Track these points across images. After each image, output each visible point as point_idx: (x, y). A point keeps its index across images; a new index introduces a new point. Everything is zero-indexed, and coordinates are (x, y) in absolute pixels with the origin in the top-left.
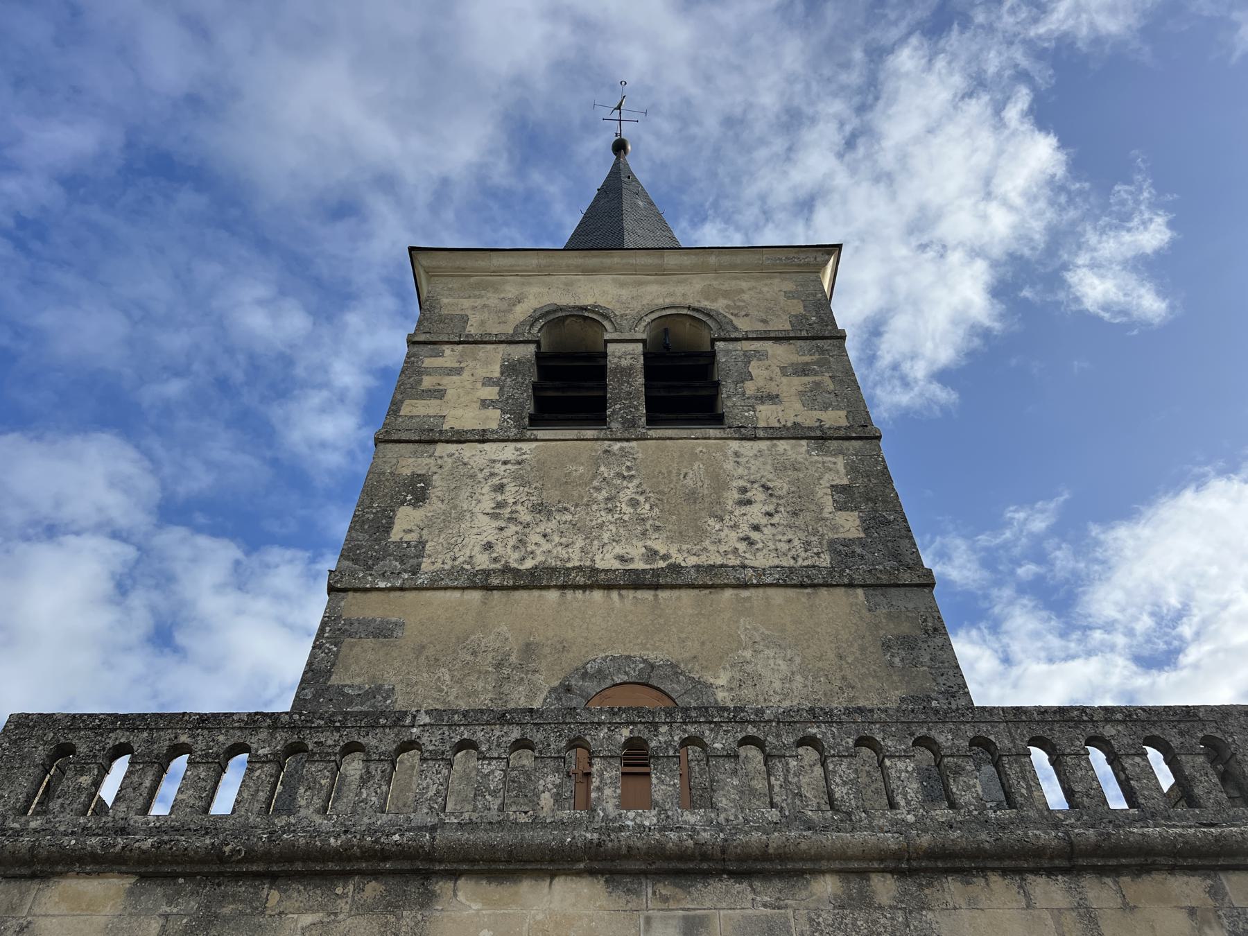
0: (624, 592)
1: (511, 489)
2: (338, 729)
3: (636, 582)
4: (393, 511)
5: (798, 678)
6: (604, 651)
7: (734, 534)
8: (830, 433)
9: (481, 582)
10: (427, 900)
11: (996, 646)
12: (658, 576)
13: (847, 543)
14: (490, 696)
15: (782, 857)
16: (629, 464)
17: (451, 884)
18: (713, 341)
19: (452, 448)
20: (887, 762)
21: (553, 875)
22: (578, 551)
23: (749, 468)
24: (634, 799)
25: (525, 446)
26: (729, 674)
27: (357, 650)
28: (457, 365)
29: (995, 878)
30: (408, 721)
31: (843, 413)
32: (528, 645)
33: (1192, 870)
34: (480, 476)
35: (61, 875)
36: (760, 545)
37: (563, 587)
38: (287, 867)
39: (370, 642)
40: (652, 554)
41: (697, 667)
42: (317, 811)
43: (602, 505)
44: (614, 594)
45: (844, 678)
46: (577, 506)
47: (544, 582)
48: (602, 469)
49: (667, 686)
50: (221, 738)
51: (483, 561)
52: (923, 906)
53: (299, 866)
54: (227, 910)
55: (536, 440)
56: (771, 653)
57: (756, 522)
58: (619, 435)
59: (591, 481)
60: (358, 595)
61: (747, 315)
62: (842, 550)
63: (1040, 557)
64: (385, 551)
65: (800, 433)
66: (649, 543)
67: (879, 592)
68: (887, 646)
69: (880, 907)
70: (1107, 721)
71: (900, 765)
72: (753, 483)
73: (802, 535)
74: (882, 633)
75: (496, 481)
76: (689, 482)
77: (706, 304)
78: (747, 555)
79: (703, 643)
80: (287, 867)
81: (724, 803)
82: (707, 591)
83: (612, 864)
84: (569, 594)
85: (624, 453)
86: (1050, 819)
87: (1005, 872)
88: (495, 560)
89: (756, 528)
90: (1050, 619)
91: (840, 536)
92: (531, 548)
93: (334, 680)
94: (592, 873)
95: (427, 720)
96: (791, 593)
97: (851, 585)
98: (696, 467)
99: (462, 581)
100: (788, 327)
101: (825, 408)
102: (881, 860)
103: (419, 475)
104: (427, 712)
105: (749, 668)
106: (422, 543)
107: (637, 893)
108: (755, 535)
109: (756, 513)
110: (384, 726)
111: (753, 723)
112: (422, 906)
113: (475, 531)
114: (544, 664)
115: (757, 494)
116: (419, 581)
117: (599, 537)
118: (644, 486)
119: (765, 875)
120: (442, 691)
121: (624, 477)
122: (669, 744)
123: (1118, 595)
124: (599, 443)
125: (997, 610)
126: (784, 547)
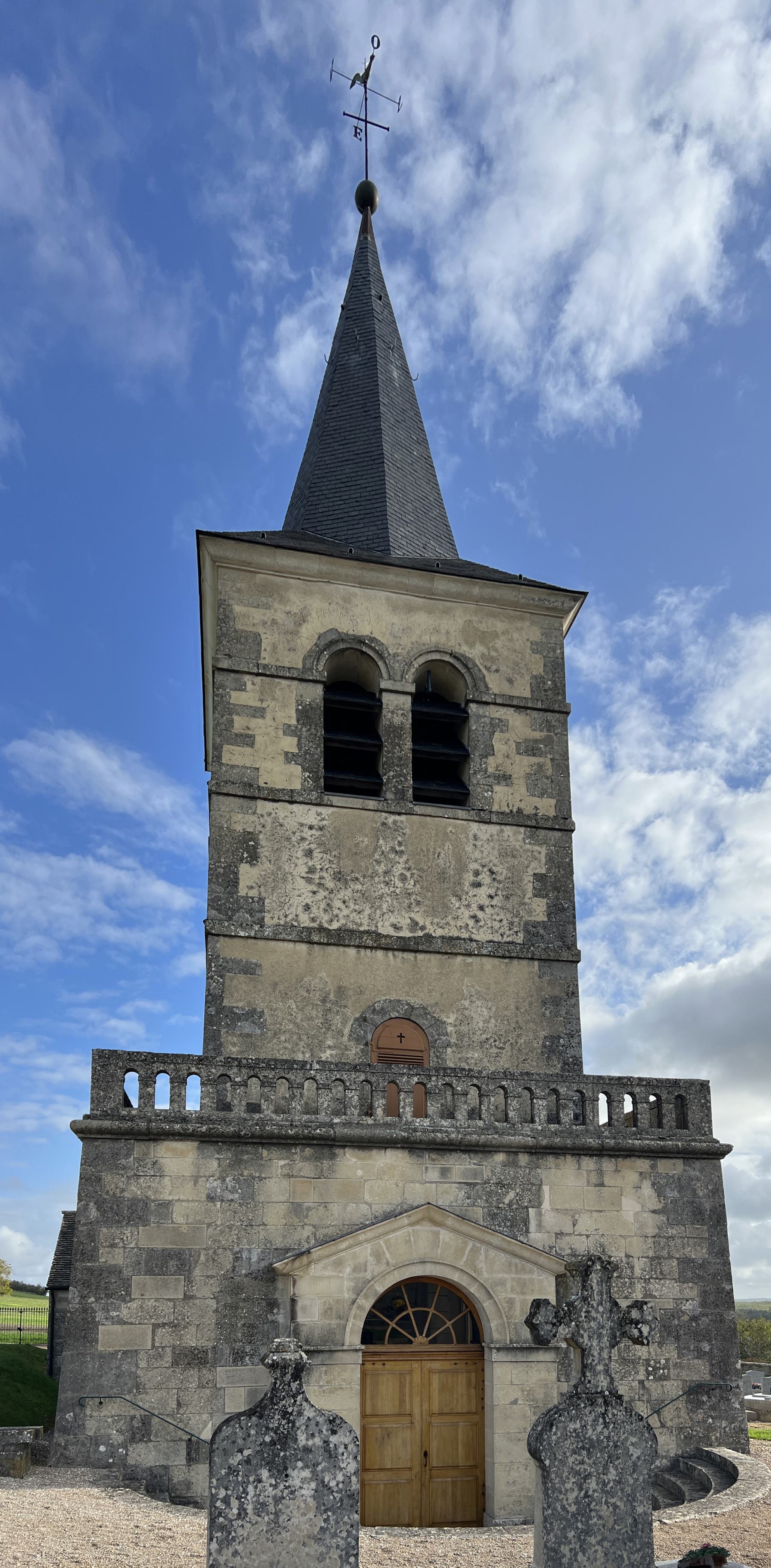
0: (396, 953)
1: (317, 854)
2: (273, 1069)
3: (405, 946)
4: (236, 867)
5: (493, 1021)
6: (384, 995)
7: (467, 912)
8: (542, 823)
9: (306, 936)
10: (333, 1156)
11: (603, 748)
12: (418, 943)
13: (535, 925)
14: (321, 1021)
15: (484, 1146)
16: (400, 839)
17: (342, 1150)
18: (468, 702)
19: (269, 806)
20: (535, 1101)
21: (386, 1148)
22: (367, 917)
23: (482, 852)
24: (420, 1112)
25: (326, 811)
26: (455, 1016)
27: (235, 982)
28: (258, 704)
29: (569, 1158)
30: (308, 1067)
31: (553, 802)
32: (340, 988)
33: (648, 1157)
34: (294, 839)
35: (164, 1140)
36: (482, 923)
37: (358, 947)
38: (269, 1141)
39: (242, 977)
40: (414, 925)
41: (438, 1010)
42: (272, 1112)
43: (382, 878)
44: (390, 954)
45: (517, 1022)
46: (364, 877)
47: (347, 942)
48: (381, 842)
49: (420, 1021)
50: (213, 1070)
51: (305, 920)
52: (538, 1167)
53: (275, 1141)
54: (245, 1157)
55: (332, 806)
56: (479, 1003)
57: (482, 903)
58: (393, 809)
59: (374, 852)
60: (226, 939)
61: (497, 671)
62: (531, 929)
63: (674, 651)
64: (238, 904)
65: (521, 821)
66: (412, 915)
67: (547, 964)
68: (544, 1003)
69: (521, 1167)
70: (638, 1085)
71: (540, 1102)
72: (484, 866)
73: (509, 916)
74: (543, 993)
75: (305, 845)
76: (441, 861)
77: (464, 650)
78: (474, 931)
79: (442, 994)
80: (269, 1141)
81: (459, 1117)
82: (446, 956)
83: (412, 1146)
84: (362, 951)
85: (397, 827)
86: (598, 1132)
87: (573, 1155)
88: (313, 920)
89: (481, 908)
90: (663, 725)
91: (533, 919)
92: (336, 912)
93: (226, 1003)
94: (403, 1148)
95: (318, 1067)
96: (496, 961)
97: (532, 959)
98: (446, 848)
99: (293, 936)
100: (527, 694)
101: (541, 796)
102: (525, 1148)
103: (249, 833)
104: (318, 1062)
105: (466, 1013)
106: (261, 900)
107: (422, 1157)
108: (480, 914)
109: (483, 891)
110: (296, 1069)
111: (477, 1078)
112: (331, 1159)
113: (297, 893)
114: (350, 1002)
115: (485, 878)
116: (266, 933)
117: (380, 907)
118: (410, 863)
119: (476, 1152)
120: (292, 1015)
121: (396, 852)
122: (436, 1086)
123: (734, 706)
124: (378, 814)
125: (615, 708)
126: (496, 925)
